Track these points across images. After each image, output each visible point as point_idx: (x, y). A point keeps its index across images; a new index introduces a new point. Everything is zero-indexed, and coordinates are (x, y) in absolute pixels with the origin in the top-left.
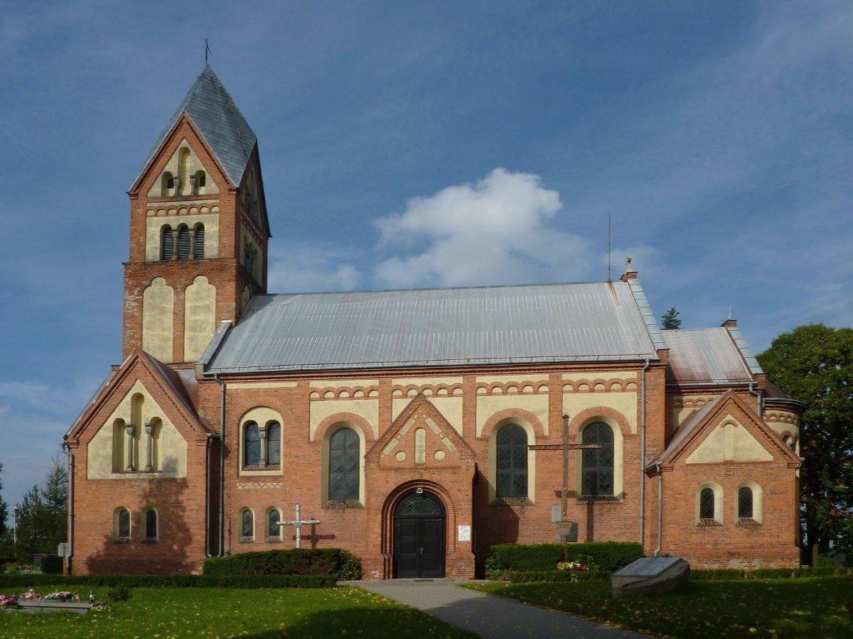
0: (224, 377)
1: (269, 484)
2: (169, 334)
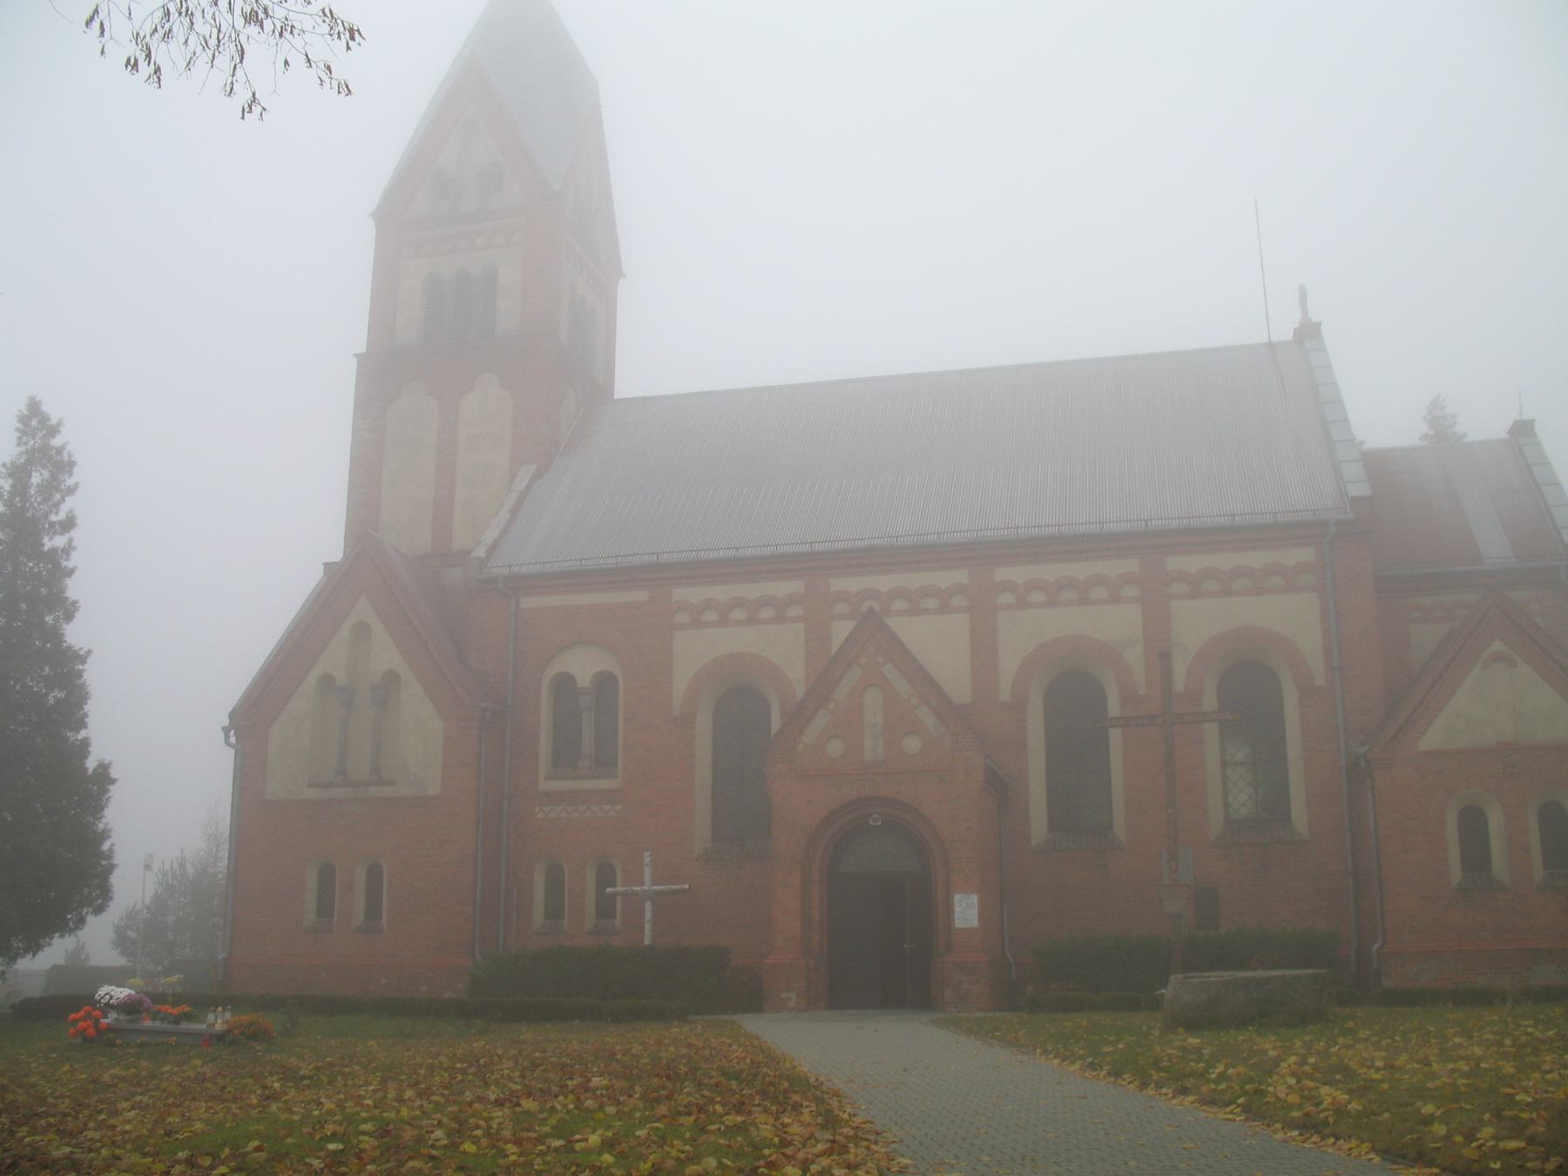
1: (595, 808)
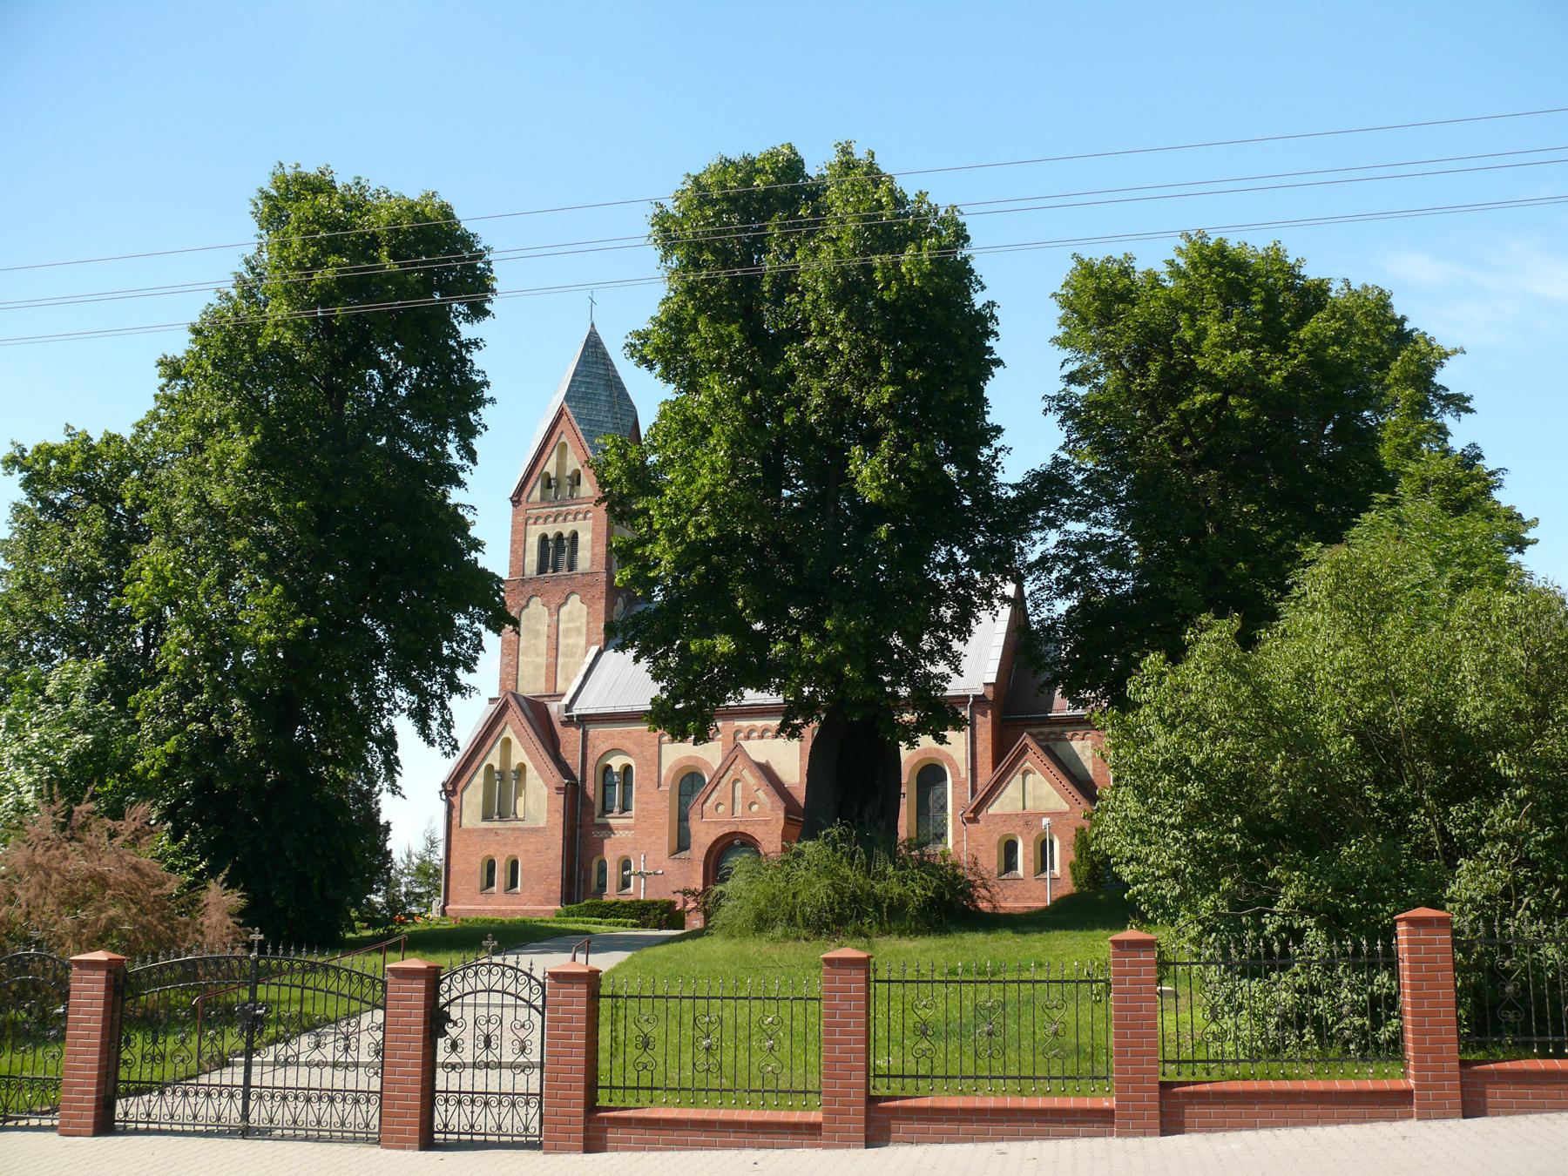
0: (585, 720)
2: (543, 660)
